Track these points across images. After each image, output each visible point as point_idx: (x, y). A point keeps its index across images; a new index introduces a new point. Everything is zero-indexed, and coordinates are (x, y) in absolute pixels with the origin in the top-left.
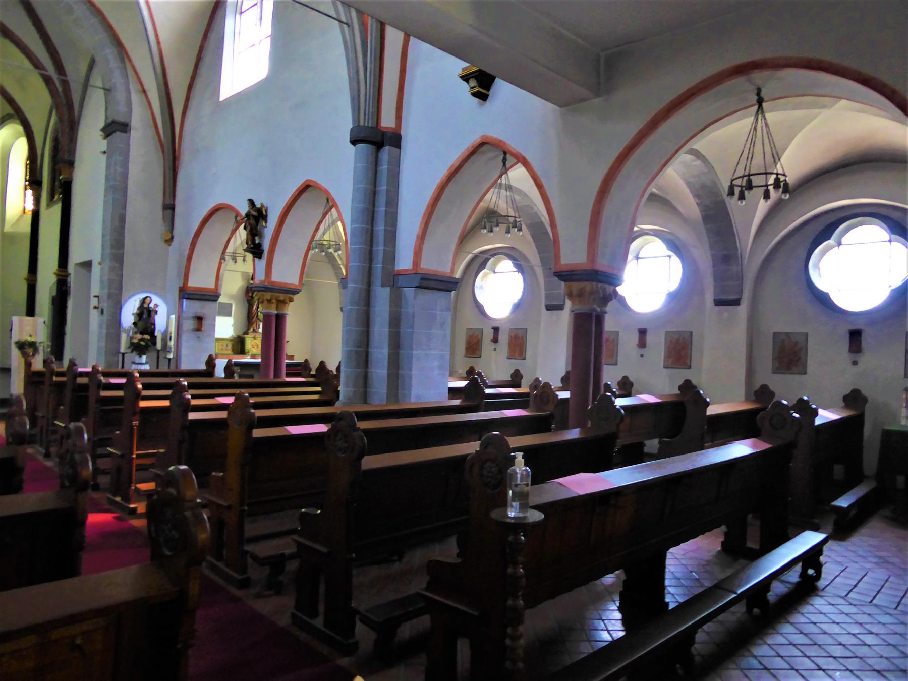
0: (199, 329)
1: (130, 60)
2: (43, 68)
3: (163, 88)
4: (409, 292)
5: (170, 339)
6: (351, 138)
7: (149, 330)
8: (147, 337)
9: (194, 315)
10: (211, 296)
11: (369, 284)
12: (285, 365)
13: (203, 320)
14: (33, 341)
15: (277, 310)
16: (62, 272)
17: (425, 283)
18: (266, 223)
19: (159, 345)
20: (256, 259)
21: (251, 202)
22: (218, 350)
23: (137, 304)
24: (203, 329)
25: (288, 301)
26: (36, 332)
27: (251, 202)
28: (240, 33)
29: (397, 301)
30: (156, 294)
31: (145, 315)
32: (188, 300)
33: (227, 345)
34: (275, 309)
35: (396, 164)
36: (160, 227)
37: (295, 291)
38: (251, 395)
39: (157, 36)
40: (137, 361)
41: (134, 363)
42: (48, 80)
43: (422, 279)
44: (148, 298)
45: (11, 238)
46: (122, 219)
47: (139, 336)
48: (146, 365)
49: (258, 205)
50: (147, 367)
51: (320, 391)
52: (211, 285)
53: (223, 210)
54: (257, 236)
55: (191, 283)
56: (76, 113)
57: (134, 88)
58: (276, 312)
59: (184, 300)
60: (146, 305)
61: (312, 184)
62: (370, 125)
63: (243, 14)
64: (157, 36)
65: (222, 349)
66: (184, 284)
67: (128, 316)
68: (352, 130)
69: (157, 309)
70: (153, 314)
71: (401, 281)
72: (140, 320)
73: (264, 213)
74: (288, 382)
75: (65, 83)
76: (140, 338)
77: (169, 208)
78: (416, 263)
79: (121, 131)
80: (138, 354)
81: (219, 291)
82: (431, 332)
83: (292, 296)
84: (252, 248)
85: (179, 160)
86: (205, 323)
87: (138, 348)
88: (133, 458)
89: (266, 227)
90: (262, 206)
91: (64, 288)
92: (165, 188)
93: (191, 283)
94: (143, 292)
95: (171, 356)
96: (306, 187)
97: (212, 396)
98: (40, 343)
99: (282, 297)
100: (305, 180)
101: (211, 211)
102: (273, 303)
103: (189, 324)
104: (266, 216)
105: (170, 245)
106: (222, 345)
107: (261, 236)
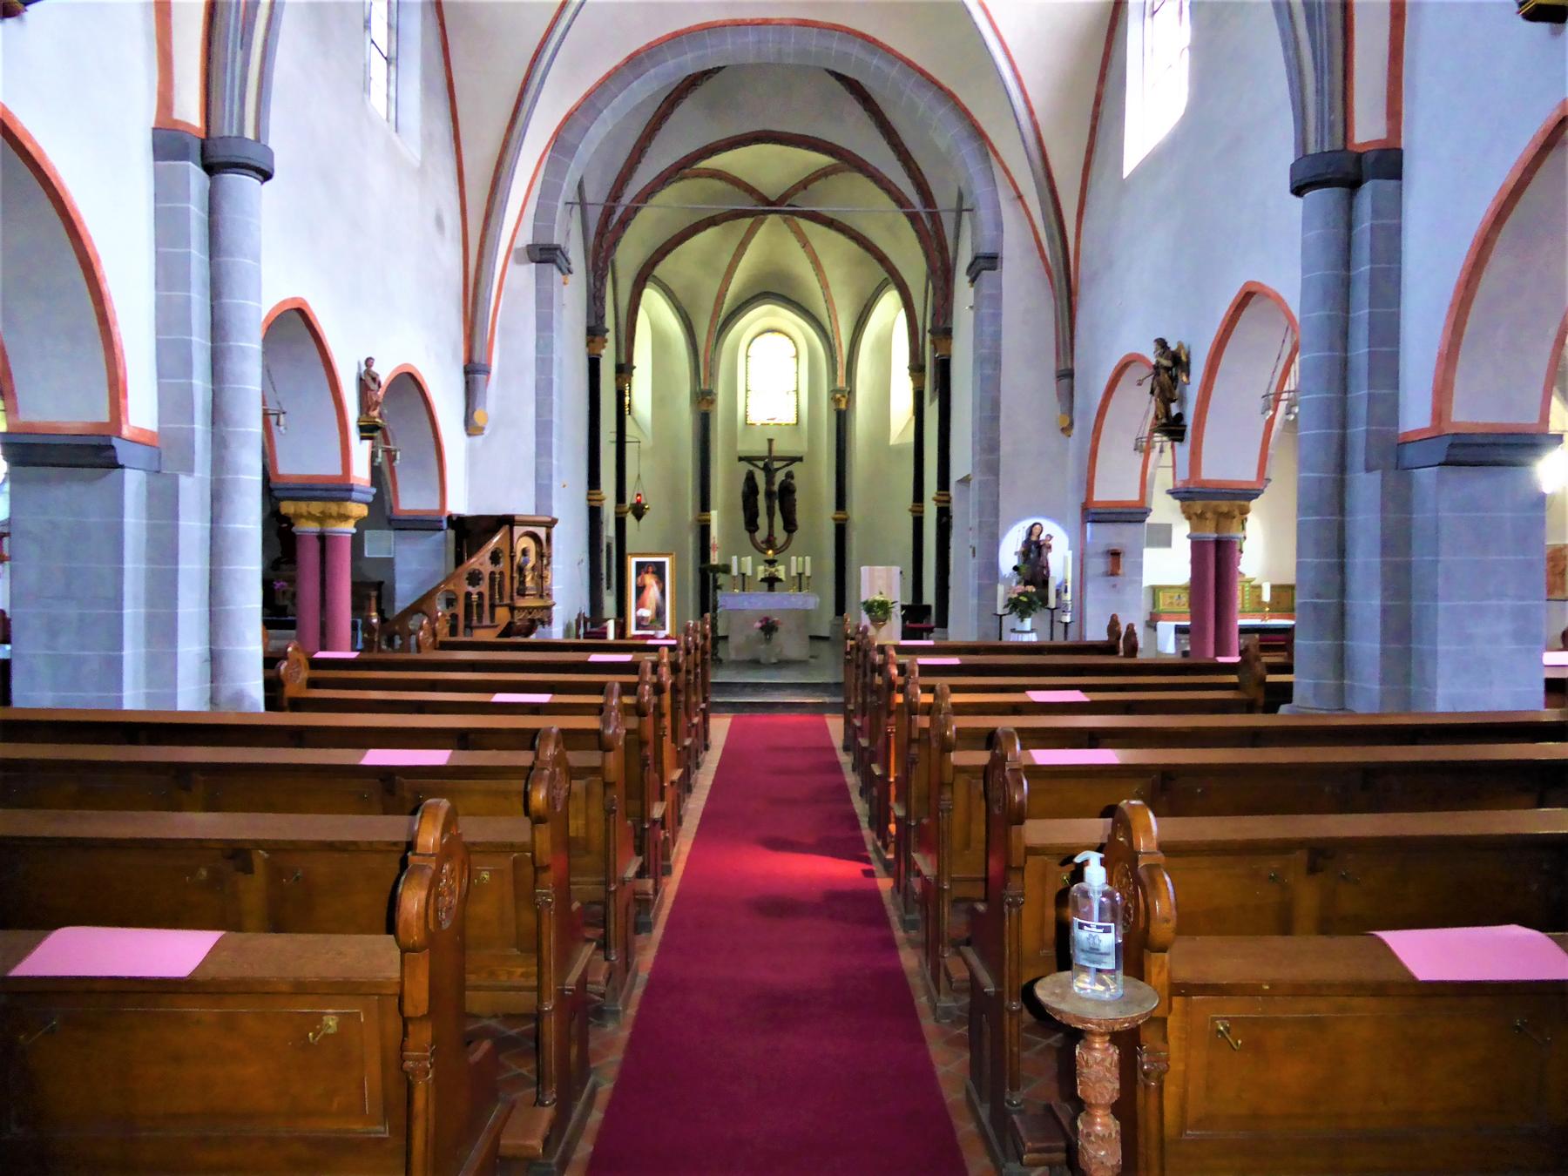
0: (1113, 572)
1: (996, 153)
2: (911, 205)
3: (1044, 183)
4: (1426, 477)
5: (1066, 591)
6: (1292, 185)
7: (1039, 579)
8: (1031, 589)
9: (1107, 549)
10: (1134, 514)
11: (1342, 467)
12: (1237, 630)
13: (1121, 556)
14: (883, 601)
15: (1217, 533)
16: (943, 495)
17: (1460, 454)
18: (1188, 376)
19: (1052, 603)
20: (1176, 444)
21: (1162, 343)
22: (1164, 605)
23: (1022, 536)
24: (1120, 572)
25: (1237, 513)
26: (890, 587)
27: (1162, 343)
28: (1152, 50)
29: (1399, 500)
30: (1048, 517)
31: (1034, 550)
32: (1094, 524)
33: (1179, 597)
34: (1213, 529)
35: (1393, 212)
36: (1054, 408)
37: (1249, 494)
38: (955, 689)
39: (1027, 101)
40: (1018, 629)
41: (1013, 631)
42: (914, 218)
43: (1452, 446)
44: (1037, 526)
45: (898, 450)
46: (995, 405)
47: (1021, 588)
48: (1030, 634)
49: (1173, 347)
50: (1032, 638)
51: (1235, 683)
52: (1132, 495)
53: (1132, 365)
54: (1174, 401)
55: (1098, 496)
56: (951, 254)
57: (1005, 196)
58: (1215, 535)
59: (1088, 525)
60: (1034, 538)
61: (1253, 289)
62: (1326, 150)
63: (1156, 15)
64: (1027, 101)
65: (1171, 603)
66: (1087, 499)
67: (1009, 555)
68: (1293, 168)
69: (1050, 542)
70: (1044, 550)
71: (1410, 453)
72: (1025, 562)
73: (1184, 358)
74: (1222, 663)
75: (935, 217)
76: (1020, 591)
77: (1066, 375)
78: (1439, 414)
79: (990, 269)
80: (1020, 617)
81: (1147, 505)
82: (1318, 560)
83: (1246, 503)
84: (1164, 425)
85: (1076, 294)
86: (1124, 561)
87: (1020, 607)
88: (891, 783)
89: (1189, 384)
90: (1180, 346)
91: (944, 519)
92: (1057, 343)
93: (1098, 496)
94: (1033, 516)
95: (1067, 619)
96: (1247, 297)
97: (1022, 689)
98: (893, 603)
99: (1224, 506)
100: (1243, 284)
101: (121, 409)
102: (1206, 519)
103: (1098, 565)
104: (1188, 363)
105: (1070, 436)
106: (1171, 597)
107: (1182, 401)
